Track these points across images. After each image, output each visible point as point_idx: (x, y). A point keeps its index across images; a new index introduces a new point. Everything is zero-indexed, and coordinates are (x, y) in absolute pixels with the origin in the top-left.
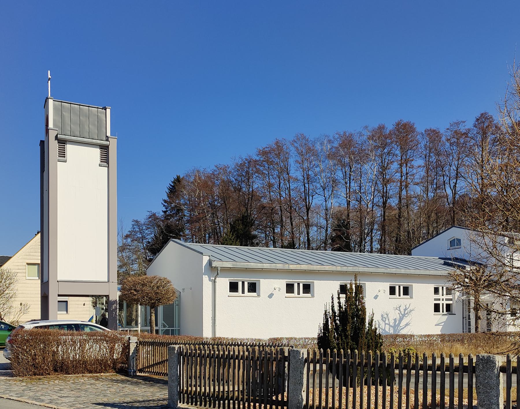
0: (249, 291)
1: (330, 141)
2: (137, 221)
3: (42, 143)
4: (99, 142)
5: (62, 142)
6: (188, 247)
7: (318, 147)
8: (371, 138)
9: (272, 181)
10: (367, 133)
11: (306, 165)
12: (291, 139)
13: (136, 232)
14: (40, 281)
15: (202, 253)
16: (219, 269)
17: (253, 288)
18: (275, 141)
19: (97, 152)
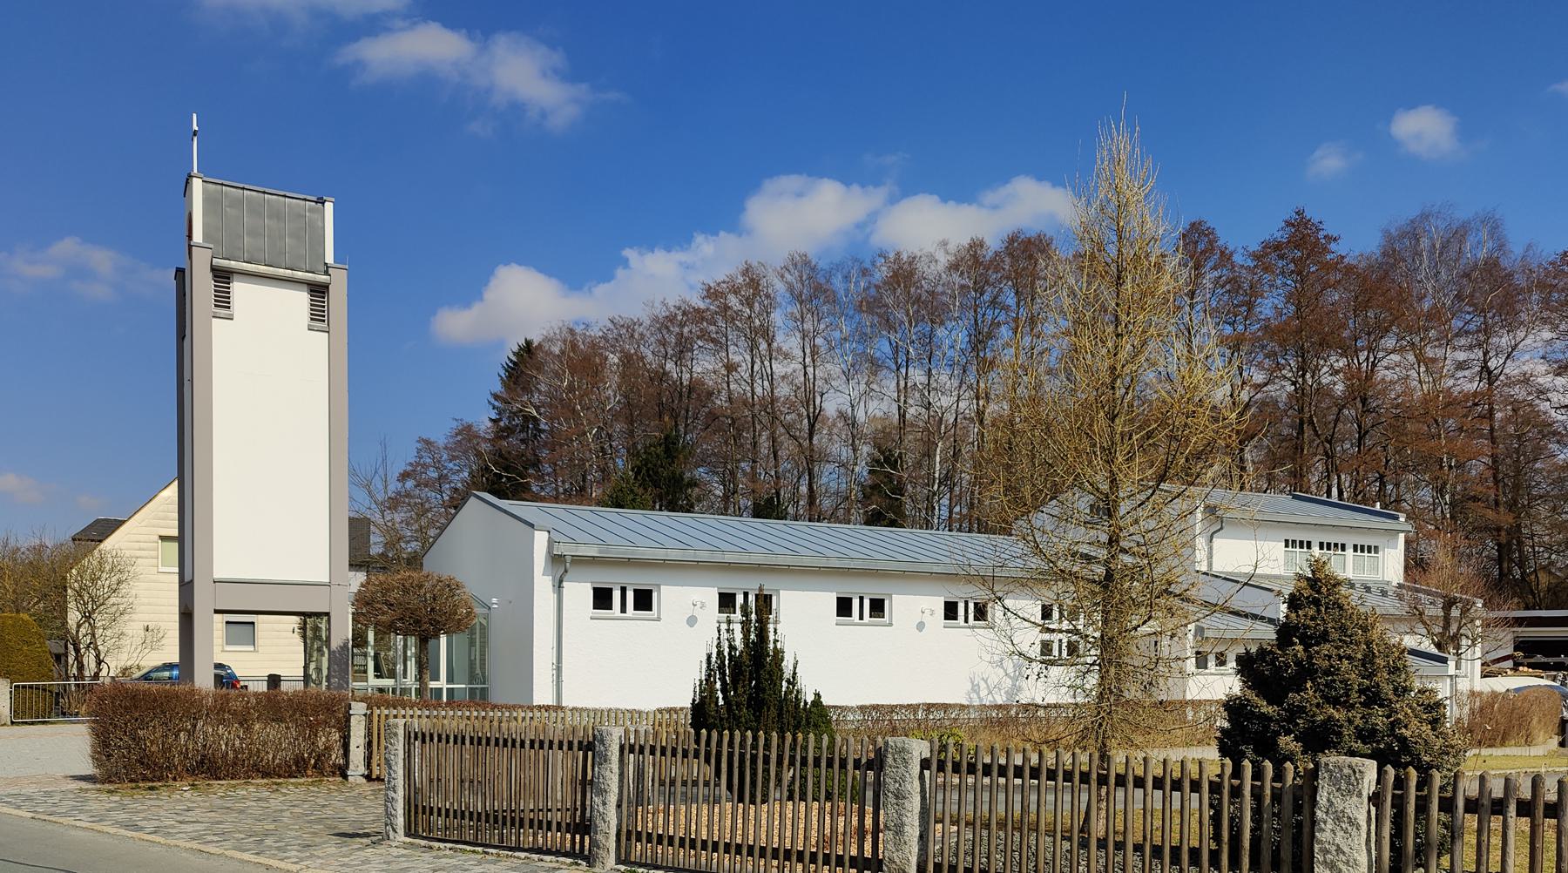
0: (976, 619)
1: (865, 272)
2: (428, 442)
3: (180, 273)
4: (309, 276)
5: (222, 276)
6: (506, 512)
7: (837, 283)
8: (954, 267)
9: (736, 359)
10: (943, 260)
11: (808, 326)
12: (779, 263)
13: (424, 466)
14: (176, 577)
15: (532, 526)
16: (568, 559)
17: (644, 600)
18: (742, 267)
19: (302, 298)
